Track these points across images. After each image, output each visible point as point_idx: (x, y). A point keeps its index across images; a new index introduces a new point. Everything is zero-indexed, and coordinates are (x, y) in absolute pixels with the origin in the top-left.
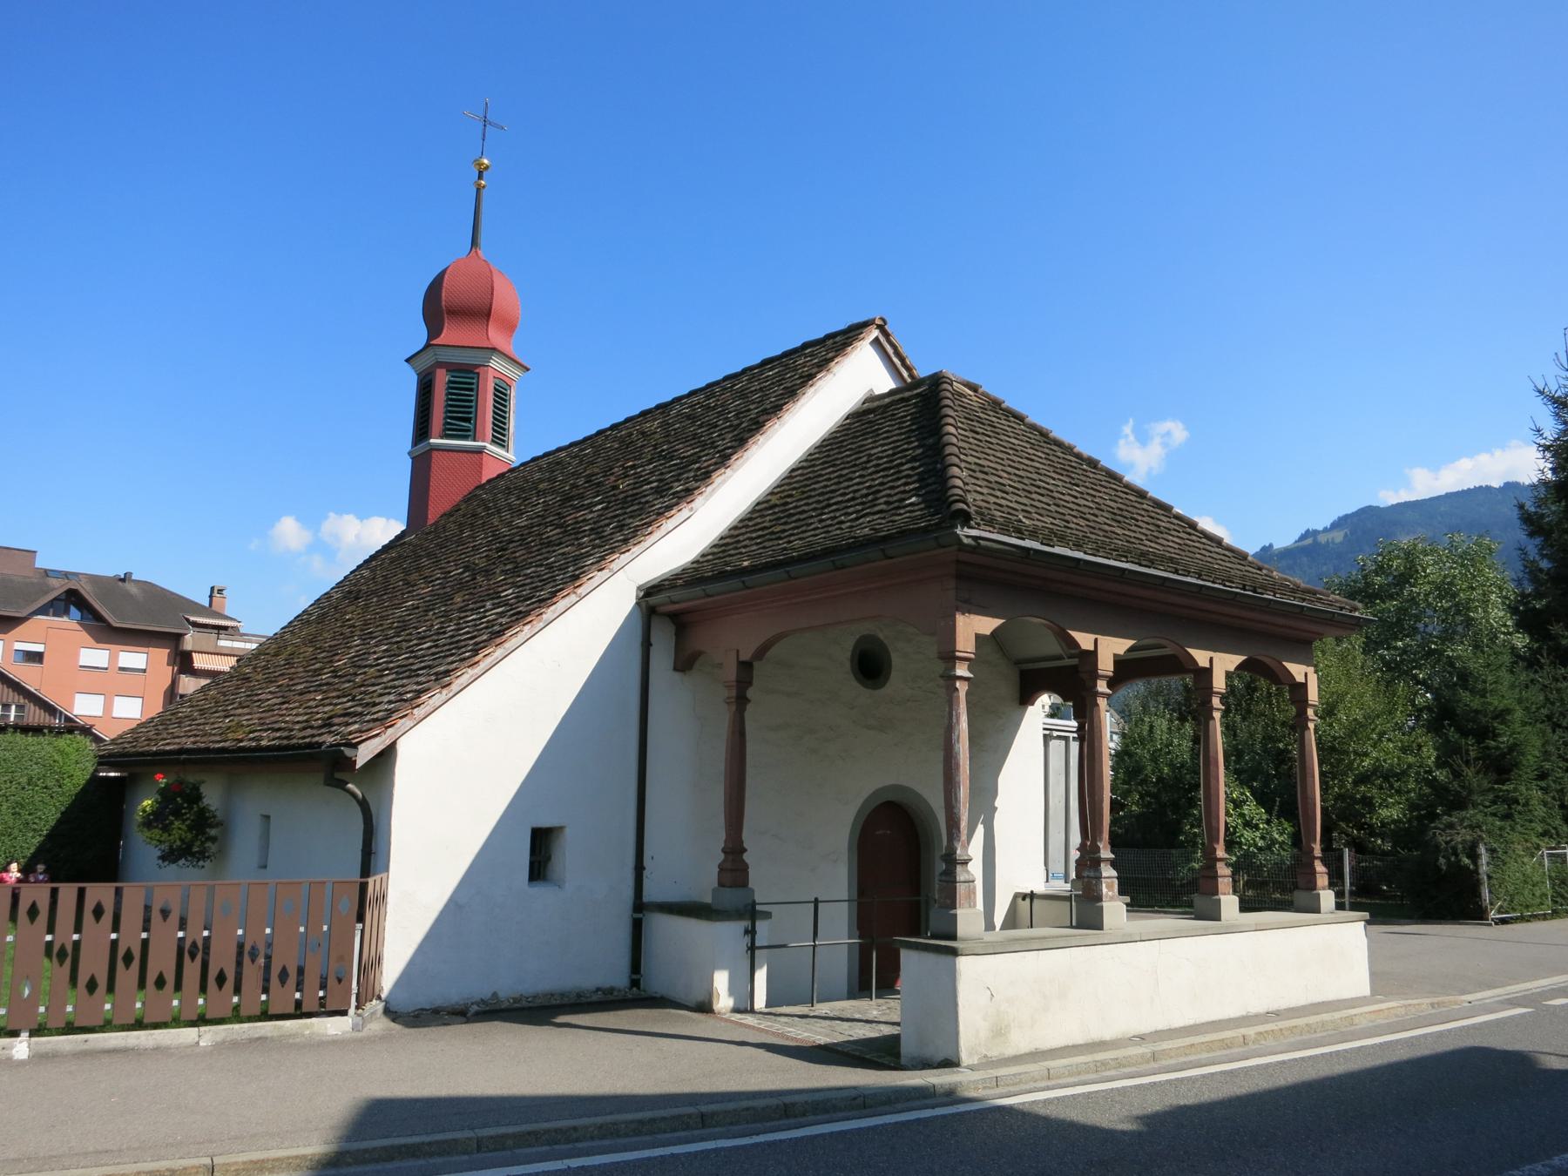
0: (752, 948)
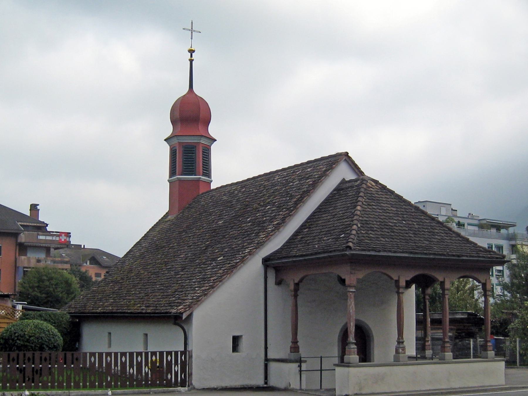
0: (301, 371)
